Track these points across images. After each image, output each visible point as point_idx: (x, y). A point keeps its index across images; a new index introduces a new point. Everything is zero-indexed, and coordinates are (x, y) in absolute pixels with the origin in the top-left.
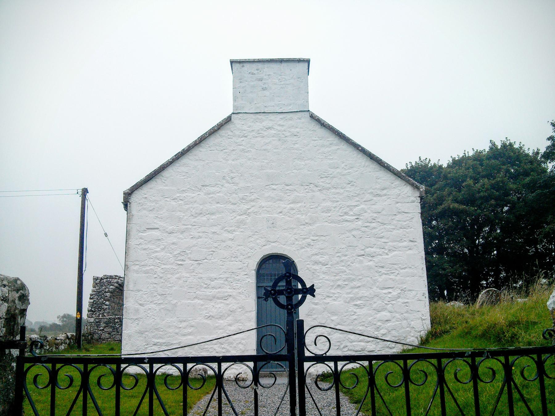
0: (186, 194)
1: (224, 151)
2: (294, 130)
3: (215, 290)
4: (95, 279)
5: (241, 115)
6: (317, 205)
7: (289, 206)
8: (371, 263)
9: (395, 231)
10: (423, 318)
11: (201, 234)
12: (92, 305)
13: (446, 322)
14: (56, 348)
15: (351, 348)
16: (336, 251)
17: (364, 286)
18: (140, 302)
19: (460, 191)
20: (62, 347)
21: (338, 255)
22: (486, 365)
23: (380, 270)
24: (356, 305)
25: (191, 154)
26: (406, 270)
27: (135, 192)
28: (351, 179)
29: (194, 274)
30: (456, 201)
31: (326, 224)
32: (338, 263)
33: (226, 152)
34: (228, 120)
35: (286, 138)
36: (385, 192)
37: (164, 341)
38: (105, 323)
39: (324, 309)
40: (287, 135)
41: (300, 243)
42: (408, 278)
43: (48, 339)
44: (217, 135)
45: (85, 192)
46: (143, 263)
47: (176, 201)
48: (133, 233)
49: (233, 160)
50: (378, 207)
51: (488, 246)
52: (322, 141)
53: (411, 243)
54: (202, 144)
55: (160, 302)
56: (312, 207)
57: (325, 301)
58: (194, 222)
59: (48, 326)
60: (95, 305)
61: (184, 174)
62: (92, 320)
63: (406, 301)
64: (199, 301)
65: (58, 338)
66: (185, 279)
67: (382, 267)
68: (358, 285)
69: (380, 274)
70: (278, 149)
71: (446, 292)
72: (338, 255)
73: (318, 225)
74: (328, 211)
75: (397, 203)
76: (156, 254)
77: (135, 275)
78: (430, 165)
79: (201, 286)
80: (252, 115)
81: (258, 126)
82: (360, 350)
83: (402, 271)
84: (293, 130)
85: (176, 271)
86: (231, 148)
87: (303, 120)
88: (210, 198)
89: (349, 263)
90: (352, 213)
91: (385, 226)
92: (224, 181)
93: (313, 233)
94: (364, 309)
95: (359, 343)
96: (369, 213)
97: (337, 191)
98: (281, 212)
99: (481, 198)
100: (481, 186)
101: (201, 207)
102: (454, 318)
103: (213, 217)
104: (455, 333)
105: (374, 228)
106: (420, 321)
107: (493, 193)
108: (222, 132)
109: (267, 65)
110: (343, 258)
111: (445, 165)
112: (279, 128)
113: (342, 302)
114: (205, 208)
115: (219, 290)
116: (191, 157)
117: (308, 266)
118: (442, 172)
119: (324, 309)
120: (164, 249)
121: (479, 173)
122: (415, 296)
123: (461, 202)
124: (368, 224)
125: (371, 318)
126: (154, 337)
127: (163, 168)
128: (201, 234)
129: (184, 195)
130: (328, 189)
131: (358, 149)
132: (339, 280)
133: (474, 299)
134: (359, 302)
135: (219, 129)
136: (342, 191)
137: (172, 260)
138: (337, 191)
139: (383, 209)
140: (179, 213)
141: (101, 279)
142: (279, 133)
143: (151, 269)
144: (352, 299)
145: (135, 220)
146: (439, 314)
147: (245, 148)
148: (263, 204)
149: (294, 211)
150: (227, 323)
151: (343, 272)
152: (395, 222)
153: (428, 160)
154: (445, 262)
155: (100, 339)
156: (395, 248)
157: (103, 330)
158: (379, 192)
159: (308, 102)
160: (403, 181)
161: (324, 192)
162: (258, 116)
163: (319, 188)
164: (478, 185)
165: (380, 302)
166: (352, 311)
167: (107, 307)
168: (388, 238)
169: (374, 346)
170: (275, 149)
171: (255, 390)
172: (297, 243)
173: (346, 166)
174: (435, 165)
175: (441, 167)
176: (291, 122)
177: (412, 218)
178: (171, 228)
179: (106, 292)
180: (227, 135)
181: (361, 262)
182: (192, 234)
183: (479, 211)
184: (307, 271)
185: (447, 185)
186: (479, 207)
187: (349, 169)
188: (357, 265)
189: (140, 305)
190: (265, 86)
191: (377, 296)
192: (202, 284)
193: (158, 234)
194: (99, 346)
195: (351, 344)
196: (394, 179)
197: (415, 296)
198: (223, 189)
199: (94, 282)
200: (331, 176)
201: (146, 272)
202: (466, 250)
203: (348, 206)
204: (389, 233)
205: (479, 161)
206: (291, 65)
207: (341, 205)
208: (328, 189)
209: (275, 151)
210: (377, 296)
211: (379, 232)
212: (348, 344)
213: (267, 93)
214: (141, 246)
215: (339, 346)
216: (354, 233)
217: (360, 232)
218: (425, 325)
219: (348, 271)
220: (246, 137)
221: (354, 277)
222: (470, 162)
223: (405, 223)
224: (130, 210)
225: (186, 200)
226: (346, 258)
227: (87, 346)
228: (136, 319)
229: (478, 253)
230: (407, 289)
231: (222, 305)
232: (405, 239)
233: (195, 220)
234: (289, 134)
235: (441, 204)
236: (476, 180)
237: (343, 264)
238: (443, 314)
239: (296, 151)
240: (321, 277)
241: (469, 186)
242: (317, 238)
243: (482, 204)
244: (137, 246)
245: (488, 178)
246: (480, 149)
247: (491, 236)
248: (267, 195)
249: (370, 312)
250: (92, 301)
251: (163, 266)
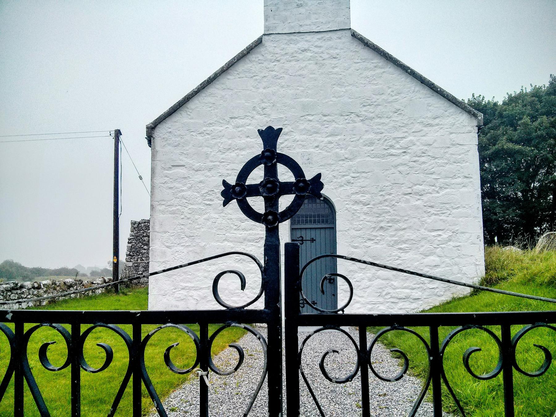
0: (213, 127)
1: (255, 78)
2: (333, 52)
3: (245, 232)
4: (133, 223)
5: (273, 36)
6: (358, 138)
7: (326, 140)
8: (418, 203)
9: (447, 166)
10: (477, 263)
11: (229, 172)
12: (130, 249)
13: (503, 268)
14: (93, 292)
15: (394, 295)
16: (379, 189)
17: (410, 228)
18: (167, 244)
19: (515, 130)
20: (99, 291)
21: (381, 193)
23: (429, 210)
24: (400, 249)
25: (218, 83)
26: (459, 210)
27: (158, 126)
28: (398, 107)
29: (223, 215)
30: (511, 140)
31: (368, 159)
32: (380, 203)
33: (256, 80)
34: (259, 42)
35: (325, 61)
36: (437, 121)
37: (192, 285)
38: (143, 267)
39: (365, 253)
40: (325, 57)
41: (339, 181)
42: (461, 219)
43: (84, 283)
44: (246, 60)
45: (118, 133)
46: (169, 203)
47: (202, 135)
48: (158, 170)
49: (264, 88)
50: (428, 139)
51: (543, 191)
52: (365, 64)
53: (465, 179)
54: (229, 71)
55: (187, 244)
56: (352, 140)
57: (365, 244)
58: (223, 158)
59: (100, 271)
60: (133, 250)
61: (211, 105)
62: (130, 264)
63: (459, 244)
64: (229, 244)
65: (94, 282)
66: (213, 220)
67: (432, 207)
68: (403, 227)
69: (429, 214)
70: (314, 74)
71: (496, 239)
72: (381, 193)
73: (359, 160)
74: (371, 144)
75: (451, 133)
76: (183, 193)
77: (162, 215)
78: (484, 103)
79: (231, 228)
80: (285, 36)
81: (292, 48)
82: (404, 297)
83: (454, 211)
84: (332, 51)
85: (204, 212)
86: (262, 75)
87: (344, 40)
88: (239, 131)
89: (394, 202)
90: (398, 146)
91: (436, 160)
92: (255, 113)
93: (353, 169)
94: (409, 253)
95: (404, 290)
96: (419, 146)
97: (382, 121)
98: (317, 147)
99: (538, 137)
100: (539, 124)
101: (230, 142)
102: (512, 264)
103: (243, 153)
104: (515, 279)
105: (424, 163)
106: (473, 266)
107: (552, 131)
108: (253, 57)
110: (387, 197)
111: (500, 103)
112: (316, 50)
113: (385, 245)
114: (235, 143)
115: (251, 232)
116: (218, 86)
117: (347, 206)
118: (496, 110)
119: (365, 253)
120: (190, 188)
121: (537, 111)
122: (468, 239)
124: (417, 158)
125: (418, 263)
126: (182, 281)
128: (229, 172)
129: (211, 128)
130: (372, 119)
131: (407, 72)
132: (382, 221)
133: (534, 244)
134: (403, 246)
135: (248, 53)
136: (388, 120)
137: (200, 200)
138: (382, 121)
139: (435, 141)
140: (206, 148)
141: (139, 223)
142: (316, 55)
143: (177, 209)
144: (397, 243)
145: (159, 157)
146: (494, 259)
147: (277, 74)
148: (298, 137)
149: (332, 145)
150: (210, 259)
151: (387, 213)
152: (447, 155)
153: (482, 97)
154: (497, 206)
155: (139, 283)
156: (447, 186)
157: (142, 274)
158: (430, 122)
159: (349, 18)
160: (459, 108)
161: (367, 122)
162: (292, 37)
163: (361, 118)
164: (536, 124)
165: (427, 245)
166: (396, 255)
167: (146, 251)
168: (439, 174)
169: (420, 293)
170: (311, 74)
171: (202, 377)
172: (335, 180)
173: (393, 91)
174: (489, 102)
175: (495, 104)
176: (329, 43)
177: (468, 151)
178: (198, 165)
179: (144, 236)
180: (257, 60)
181: (408, 201)
182: (220, 171)
183: (536, 151)
184: (346, 211)
185: (503, 123)
186: (536, 147)
187: (396, 95)
188: (403, 205)
189: (168, 247)
190: (300, 2)
191: (424, 239)
192: (232, 226)
193: (185, 172)
194: (137, 290)
195: (394, 291)
196: (448, 105)
197: (468, 239)
198: (254, 121)
199: (132, 226)
200: (375, 104)
201: (173, 213)
202: (520, 194)
203: (394, 138)
204: (441, 168)
205: (537, 97)
207: (386, 137)
208: (372, 119)
209: (311, 76)
210: (424, 239)
211: (430, 167)
212: (391, 291)
213: (302, 10)
214: (166, 185)
215: (380, 292)
216: (401, 168)
217: (407, 168)
218: (478, 271)
219: (392, 212)
220: (278, 61)
221: (398, 218)
222: (529, 99)
223: (460, 157)
224: (154, 145)
225: (213, 134)
226: (390, 197)
227: (125, 290)
228: (164, 262)
229: (532, 196)
230: (459, 231)
231: (253, 247)
232: (459, 175)
233: (223, 156)
234: (328, 56)
235: (494, 145)
236: (534, 118)
237: (387, 203)
238: (499, 260)
239: (335, 76)
240: (362, 218)
241: (526, 124)
242: (358, 175)
243: (539, 143)
244: (162, 185)
245: (547, 116)
246: (539, 85)
247: (548, 178)
248: (302, 127)
249: (417, 256)
250: (130, 245)
251: (190, 207)
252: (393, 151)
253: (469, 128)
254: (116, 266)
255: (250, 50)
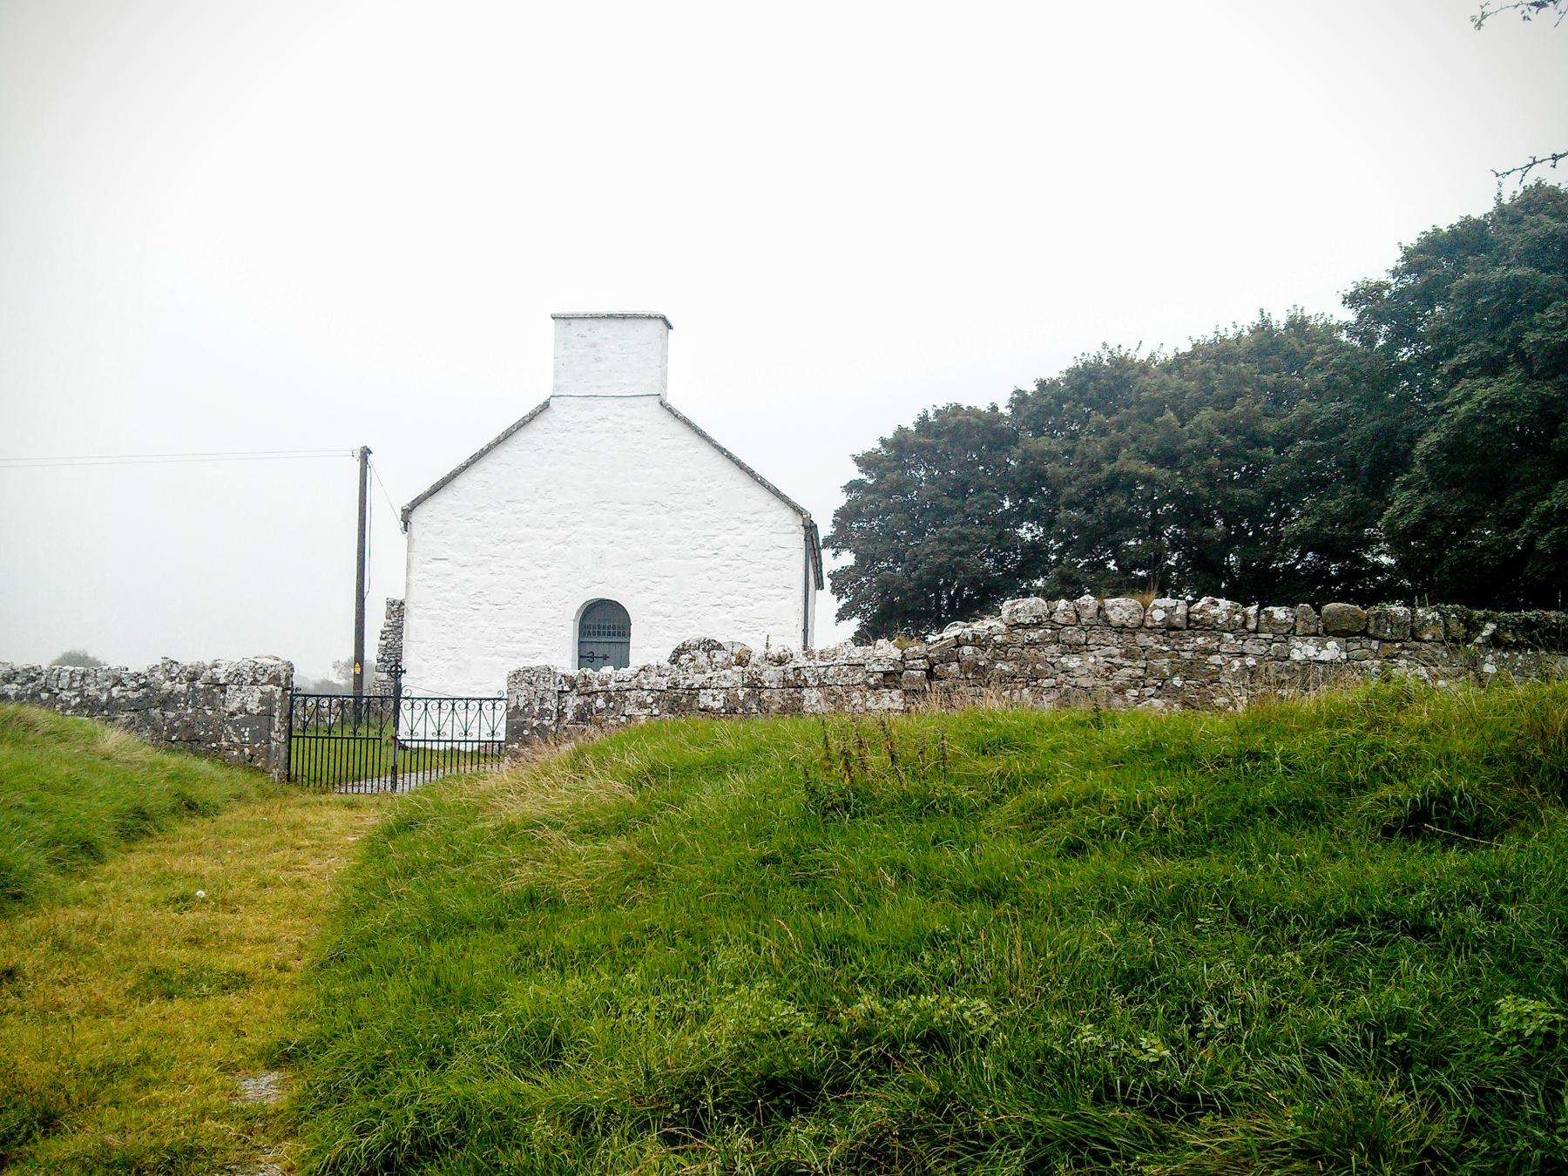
22: (485, 704)
34: (546, 406)
36: (757, 517)
44: (529, 427)
45: (366, 453)
48: (415, 564)
74: (677, 541)
108: (536, 424)
109: (604, 322)
123: (1152, 460)
127: (454, 475)
206: (638, 323)
216: (710, 573)
252: (702, 552)
253: (793, 528)
254: (359, 679)
255: (532, 417)
